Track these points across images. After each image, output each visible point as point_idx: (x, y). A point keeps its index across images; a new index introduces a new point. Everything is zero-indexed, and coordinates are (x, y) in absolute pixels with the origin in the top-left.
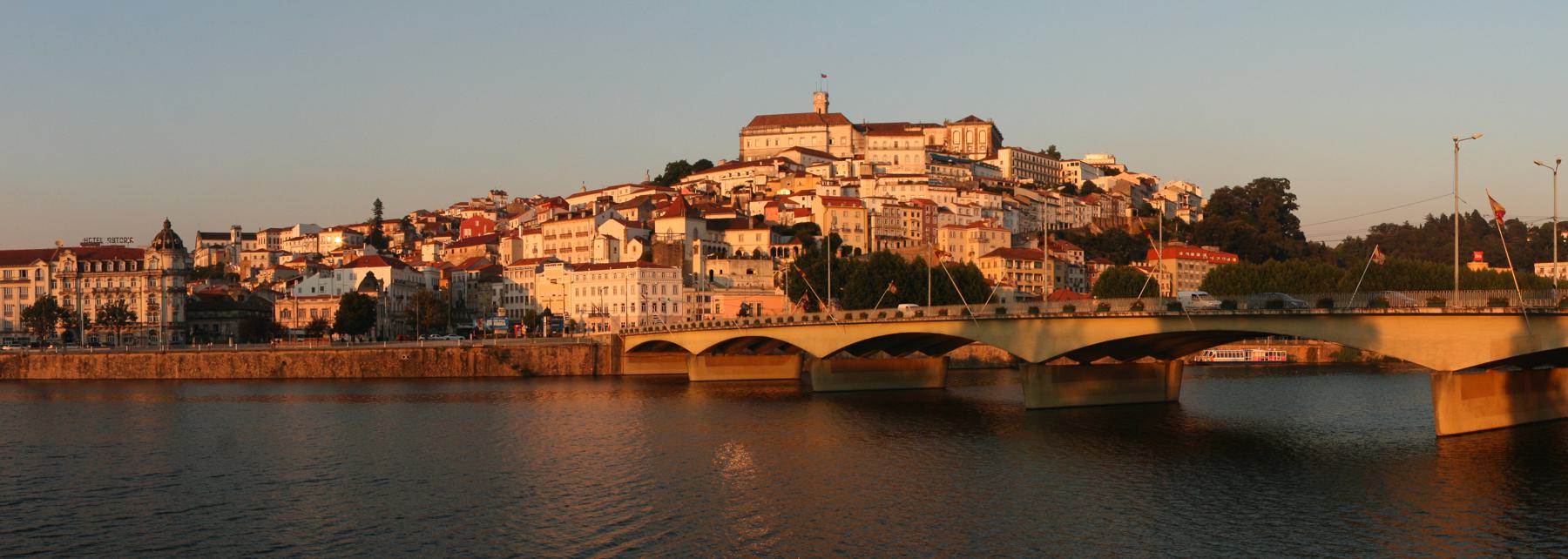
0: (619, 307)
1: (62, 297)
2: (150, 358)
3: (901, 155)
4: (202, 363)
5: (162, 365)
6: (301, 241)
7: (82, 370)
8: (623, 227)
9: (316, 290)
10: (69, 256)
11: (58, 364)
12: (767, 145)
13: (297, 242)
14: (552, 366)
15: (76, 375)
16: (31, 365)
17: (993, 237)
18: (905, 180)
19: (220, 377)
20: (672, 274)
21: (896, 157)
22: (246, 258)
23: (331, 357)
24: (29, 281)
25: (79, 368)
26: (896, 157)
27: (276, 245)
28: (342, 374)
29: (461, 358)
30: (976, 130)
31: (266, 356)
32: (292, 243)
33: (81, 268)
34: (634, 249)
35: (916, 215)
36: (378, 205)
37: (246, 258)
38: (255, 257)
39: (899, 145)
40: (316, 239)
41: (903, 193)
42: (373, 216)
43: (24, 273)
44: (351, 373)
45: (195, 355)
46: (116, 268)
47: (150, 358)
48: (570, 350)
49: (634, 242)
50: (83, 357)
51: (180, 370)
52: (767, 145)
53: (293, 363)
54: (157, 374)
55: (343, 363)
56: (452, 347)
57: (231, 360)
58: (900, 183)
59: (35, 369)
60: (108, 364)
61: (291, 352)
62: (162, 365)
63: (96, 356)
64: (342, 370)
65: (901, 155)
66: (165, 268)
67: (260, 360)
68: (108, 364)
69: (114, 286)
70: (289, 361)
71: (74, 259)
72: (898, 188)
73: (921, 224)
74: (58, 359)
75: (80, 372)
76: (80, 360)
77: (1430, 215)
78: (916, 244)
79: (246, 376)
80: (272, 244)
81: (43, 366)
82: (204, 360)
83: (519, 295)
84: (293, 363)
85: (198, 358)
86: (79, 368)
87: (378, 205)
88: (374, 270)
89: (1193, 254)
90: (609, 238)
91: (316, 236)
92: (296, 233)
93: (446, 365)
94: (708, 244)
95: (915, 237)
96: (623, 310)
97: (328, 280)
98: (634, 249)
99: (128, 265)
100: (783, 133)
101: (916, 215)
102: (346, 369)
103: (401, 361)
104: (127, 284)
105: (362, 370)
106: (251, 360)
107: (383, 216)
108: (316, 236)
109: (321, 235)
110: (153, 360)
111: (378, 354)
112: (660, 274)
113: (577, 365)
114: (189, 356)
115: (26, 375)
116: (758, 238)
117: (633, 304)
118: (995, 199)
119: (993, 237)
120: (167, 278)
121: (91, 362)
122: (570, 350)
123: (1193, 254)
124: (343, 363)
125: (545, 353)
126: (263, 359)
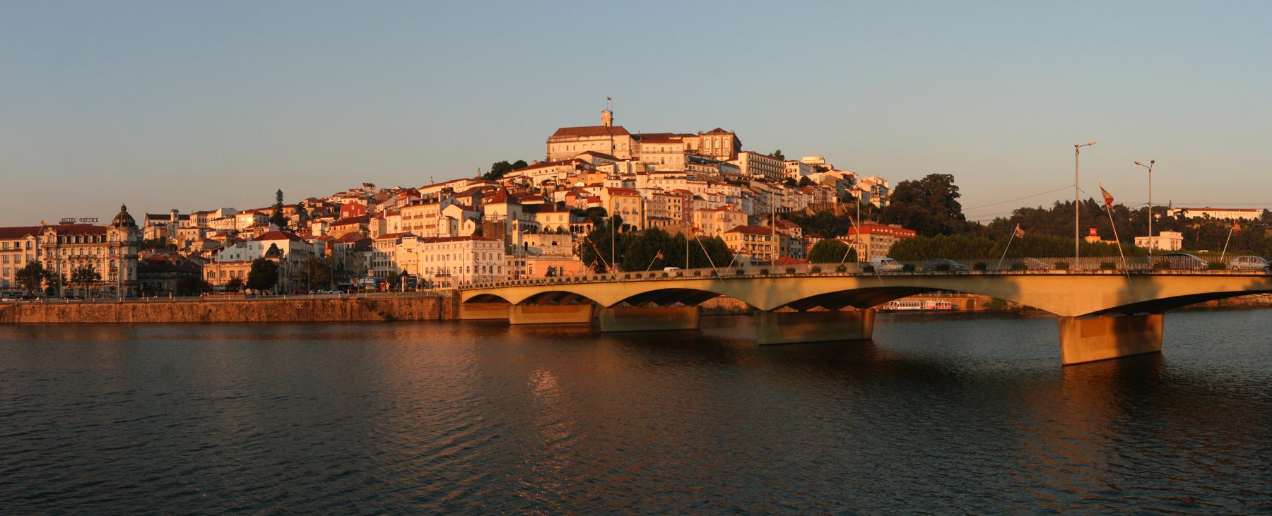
0: (458, 269)
1: (46, 262)
2: (111, 307)
3: (667, 157)
4: (149, 311)
5: (120, 313)
6: (223, 221)
7: (61, 316)
8: (461, 210)
9: (234, 257)
10: (52, 232)
11: (43, 312)
12: (568, 149)
13: (220, 221)
14: (408, 313)
15: (56, 320)
16: (23, 312)
17: (735, 218)
18: (670, 175)
19: (163, 321)
20: (497, 245)
21: (663, 159)
22: (182, 233)
23: (244, 307)
24: (21, 250)
25: (59, 314)
26: (663, 159)
27: (204, 223)
28: (253, 319)
29: (341, 307)
30: (722, 139)
31: (197, 305)
32: (216, 222)
33: (60, 241)
34: (469, 227)
35: (677, 201)
36: (280, 194)
37: (182, 233)
38: (189, 233)
39: (665, 150)
40: (233, 219)
41: (668, 185)
42: (276, 202)
43: (18, 244)
44: (260, 318)
45: (144, 304)
46: (86, 241)
47: (111, 307)
48: (422, 302)
49: (469, 222)
50: (62, 306)
51: (133, 316)
52: (568, 149)
53: (217, 311)
54: (116, 319)
55: (253, 311)
56: (334, 299)
57: (171, 308)
58: (666, 178)
59: (27, 315)
60: (80, 312)
61: (215, 303)
62: (120, 313)
63: (71, 306)
64: (252, 316)
65: (667, 157)
66: (122, 241)
67: (192, 308)
68: (80, 312)
69: (84, 254)
70: (214, 309)
71: (55, 234)
72: (664, 181)
73: (681, 209)
74: (43, 308)
75: (59, 317)
76: (59, 309)
77: (147, 214)
78: (677, 223)
79: (183, 320)
80: (201, 223)
81: (32, 313)
82: (151, 308)
83: (384, 261)
84: (217, 311)
85: (146, 307)
86: (59, 314)
87: (280, 194)
88: (276, 242)
89: (882, 231)
90: (451, 218)
91: (234, 217)
92: (219, 214)
93: (330, 312)
94: (523, 223)
95: (677, 218)
96: (461, 271)
97: (243, 249)
98: (469, 227)
99: (86, 239)
100: (579, 141)
101: (677, 201)
102: (256, 315)
103: (297, 309)
104: (94, 252)
105: (268, 316)
106: (185, 308)
107: (283, 202)
108: (234, 217)
109: (237, 216)
110: (113, 309)
111: (279, 304)
112: (488, 245)
113: (427, 312)
114: (140, 305)
115: (19, 320)
116: (561, 219)
117: (455, 268)
118: (736, 190)
119: (735, 218)
120: (124, 248)
121: (67, 310)
122: (422, 302)
123: (882, 231)
124: (253, 311)
125: (403, 303)
126: (195, 307)
